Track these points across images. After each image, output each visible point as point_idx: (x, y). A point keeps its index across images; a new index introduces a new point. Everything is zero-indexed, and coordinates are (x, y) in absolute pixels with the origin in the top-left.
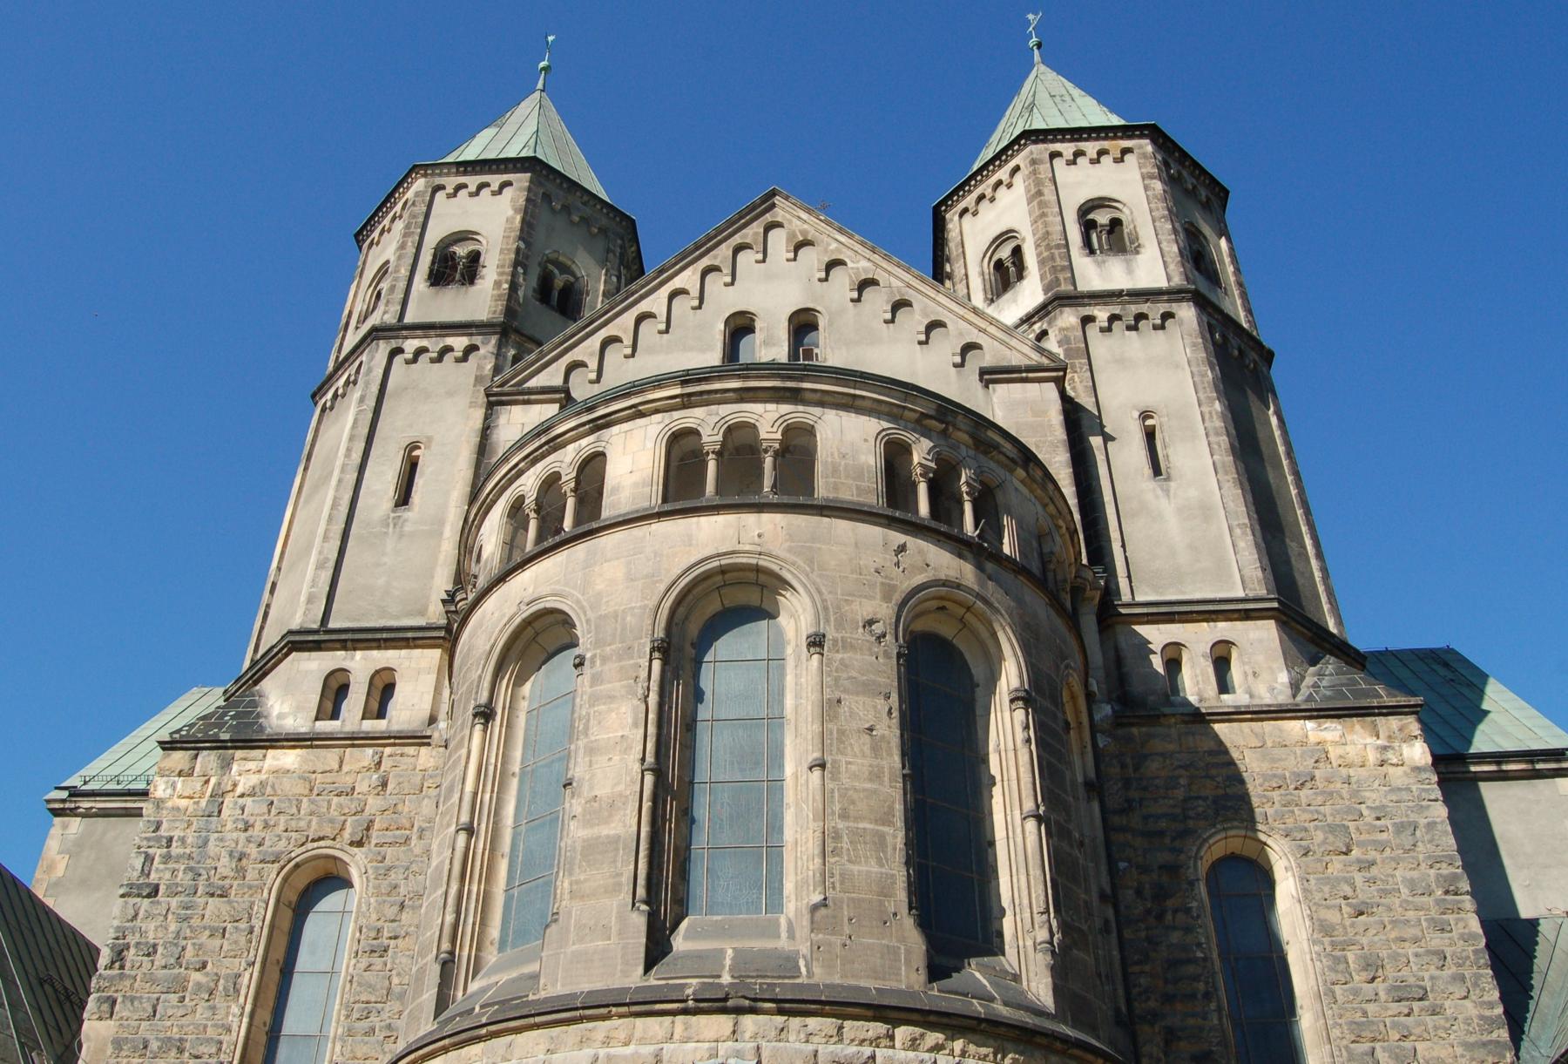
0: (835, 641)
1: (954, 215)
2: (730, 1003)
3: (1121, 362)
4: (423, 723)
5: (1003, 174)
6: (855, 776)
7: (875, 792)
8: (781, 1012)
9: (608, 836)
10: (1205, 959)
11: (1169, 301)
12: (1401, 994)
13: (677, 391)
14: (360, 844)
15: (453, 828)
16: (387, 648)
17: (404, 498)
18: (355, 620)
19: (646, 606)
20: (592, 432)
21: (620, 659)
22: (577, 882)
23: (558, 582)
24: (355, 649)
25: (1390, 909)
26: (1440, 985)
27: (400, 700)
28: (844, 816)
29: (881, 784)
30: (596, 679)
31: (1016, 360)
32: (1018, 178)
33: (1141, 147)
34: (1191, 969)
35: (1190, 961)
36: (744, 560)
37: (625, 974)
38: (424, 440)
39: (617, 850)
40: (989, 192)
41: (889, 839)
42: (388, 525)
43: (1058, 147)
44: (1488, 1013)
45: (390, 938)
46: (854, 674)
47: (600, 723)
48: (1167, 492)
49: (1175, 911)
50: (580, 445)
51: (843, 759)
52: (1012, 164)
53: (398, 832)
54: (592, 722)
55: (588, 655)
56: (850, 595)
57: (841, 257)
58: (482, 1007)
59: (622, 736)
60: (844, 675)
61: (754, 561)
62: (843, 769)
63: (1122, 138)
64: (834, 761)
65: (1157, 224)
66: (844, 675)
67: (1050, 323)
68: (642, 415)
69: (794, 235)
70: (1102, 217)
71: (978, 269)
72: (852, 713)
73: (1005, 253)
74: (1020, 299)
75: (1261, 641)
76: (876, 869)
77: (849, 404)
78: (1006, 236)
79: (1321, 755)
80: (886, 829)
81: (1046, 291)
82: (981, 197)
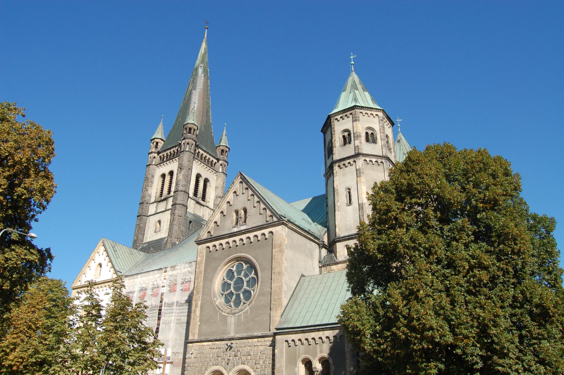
73: (370, 132)
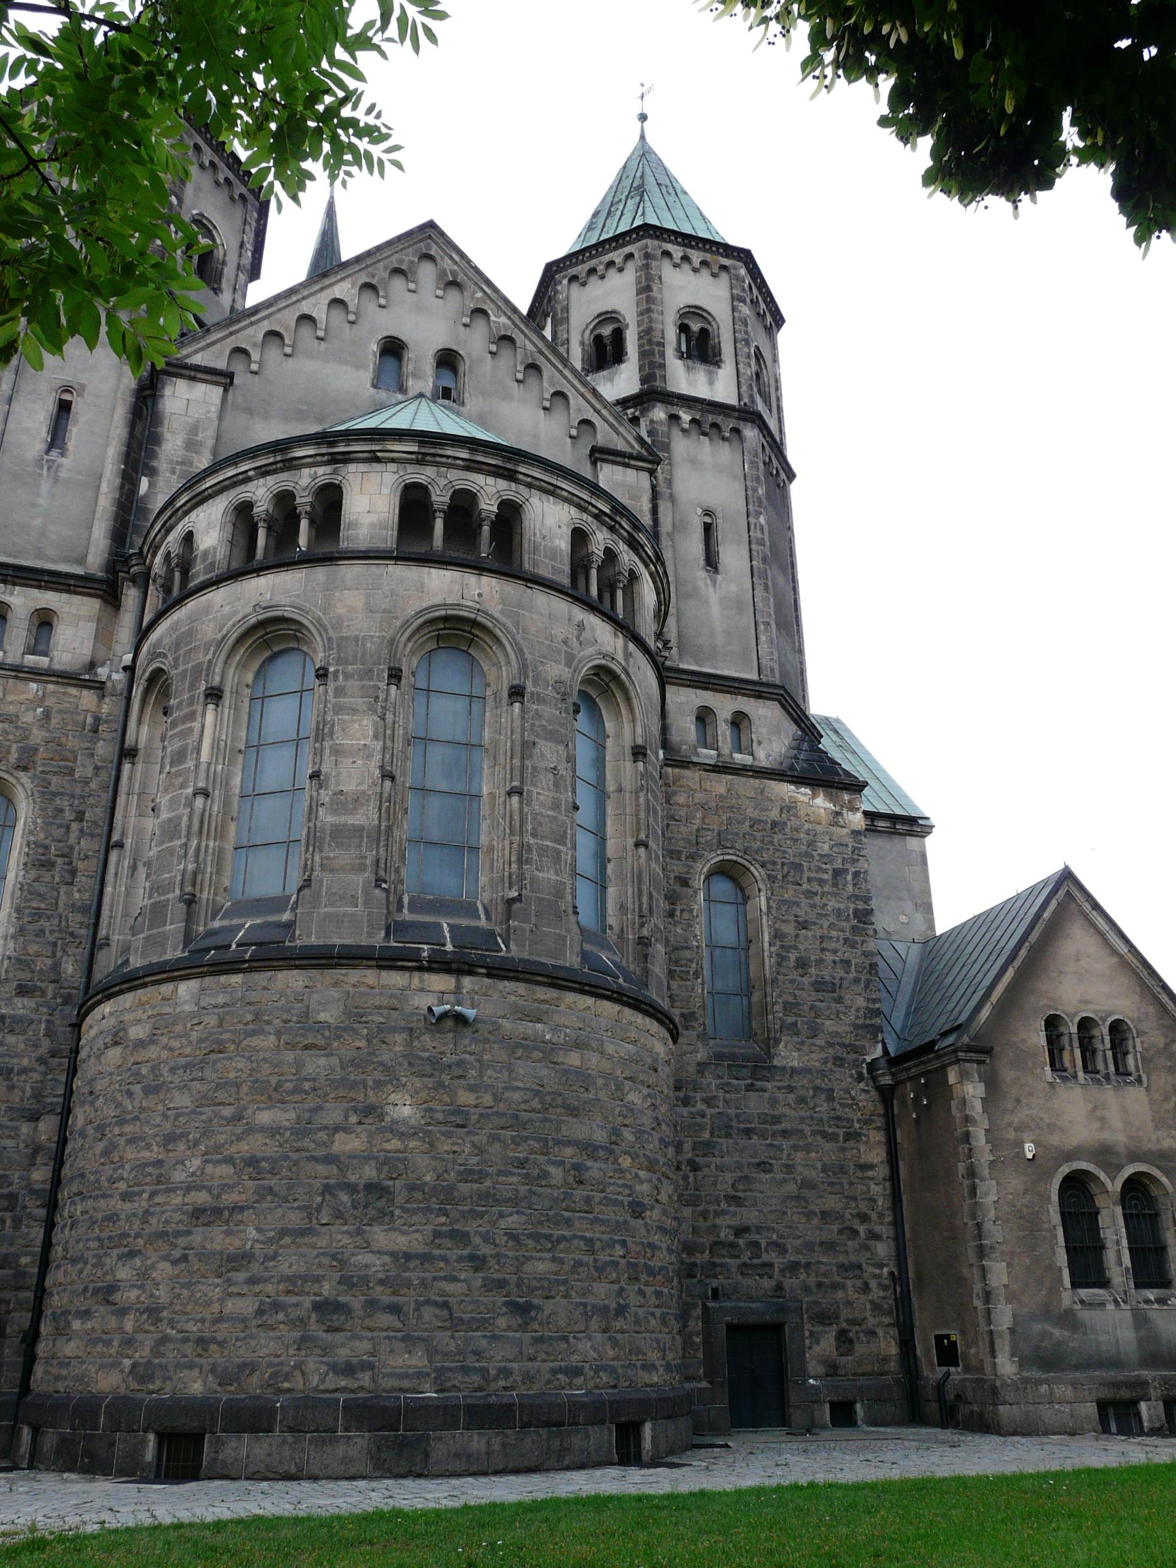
0: (532, 694)
1: (564, 277)
2: (454, 966)
3: (694, 462)
4: (84, 667)
5: (617, 256)
6: (542, 805)
7: (555, 818)
8: (488, 975)
9: (353, 825)
10: (698, 947)
11: (739, 418)
12: (820, 986)
13: (416, 449)
14: (25, 769)
15: (190, 790)
16: (47, 588)
17: (57, 437)
18: (11, 555)
19: (384, 637)
20: (328, 463)
21: (361, 679)
22: (328, 858)
23: (298, 596)
24: (14, 584)
25: (821, 927)
26: (846, 984)
27: (61, 642)
28: (534, 835)
29: (560, 813)
30: (339, 692)
31: (621, 446)
32: (631, 267)
33: (735, 268)
34: (687, 954)
35: (687, 948)
36: (465, 614)
37: (371, 935)
38: (76, 387)
39: (362, 837)
40: (601, 268)
41: (563, 856)
42: (42, 467)
43: (670, 247)
44: (871, 1006)
45: (57, 856)
46: (544, 723)
47: (344, 730)
48: (714, 582)
49: (682, 911)
50: (315, 473)
51: (535, 790)
52: (628, 249)
53: (63, 763)
54: (336, 728)
55: (331, 669)
56: (544, 658)
57: (485, 307)
58: (238, 945)
59: (365, 745)
60: (538, 723)
61: (473, 616)
62: (534, 798)
63: (722, 255)
64: (529, 791)
65: (738, 345)
66: (538, 723)
67: (643, 413)
68: (378, 460)
69: (446, 274)
70: (695, 327)
71: (579, 338)
72: (542, 754)
73: (606, 331)
74: (616, 379)
75: (766, 717)
76: (554, 877)
77: (551, 491)
78: (608, 317)
79: (789, 808)
80: (561, 847)
81: (644, 380)
82: (592, 271)
